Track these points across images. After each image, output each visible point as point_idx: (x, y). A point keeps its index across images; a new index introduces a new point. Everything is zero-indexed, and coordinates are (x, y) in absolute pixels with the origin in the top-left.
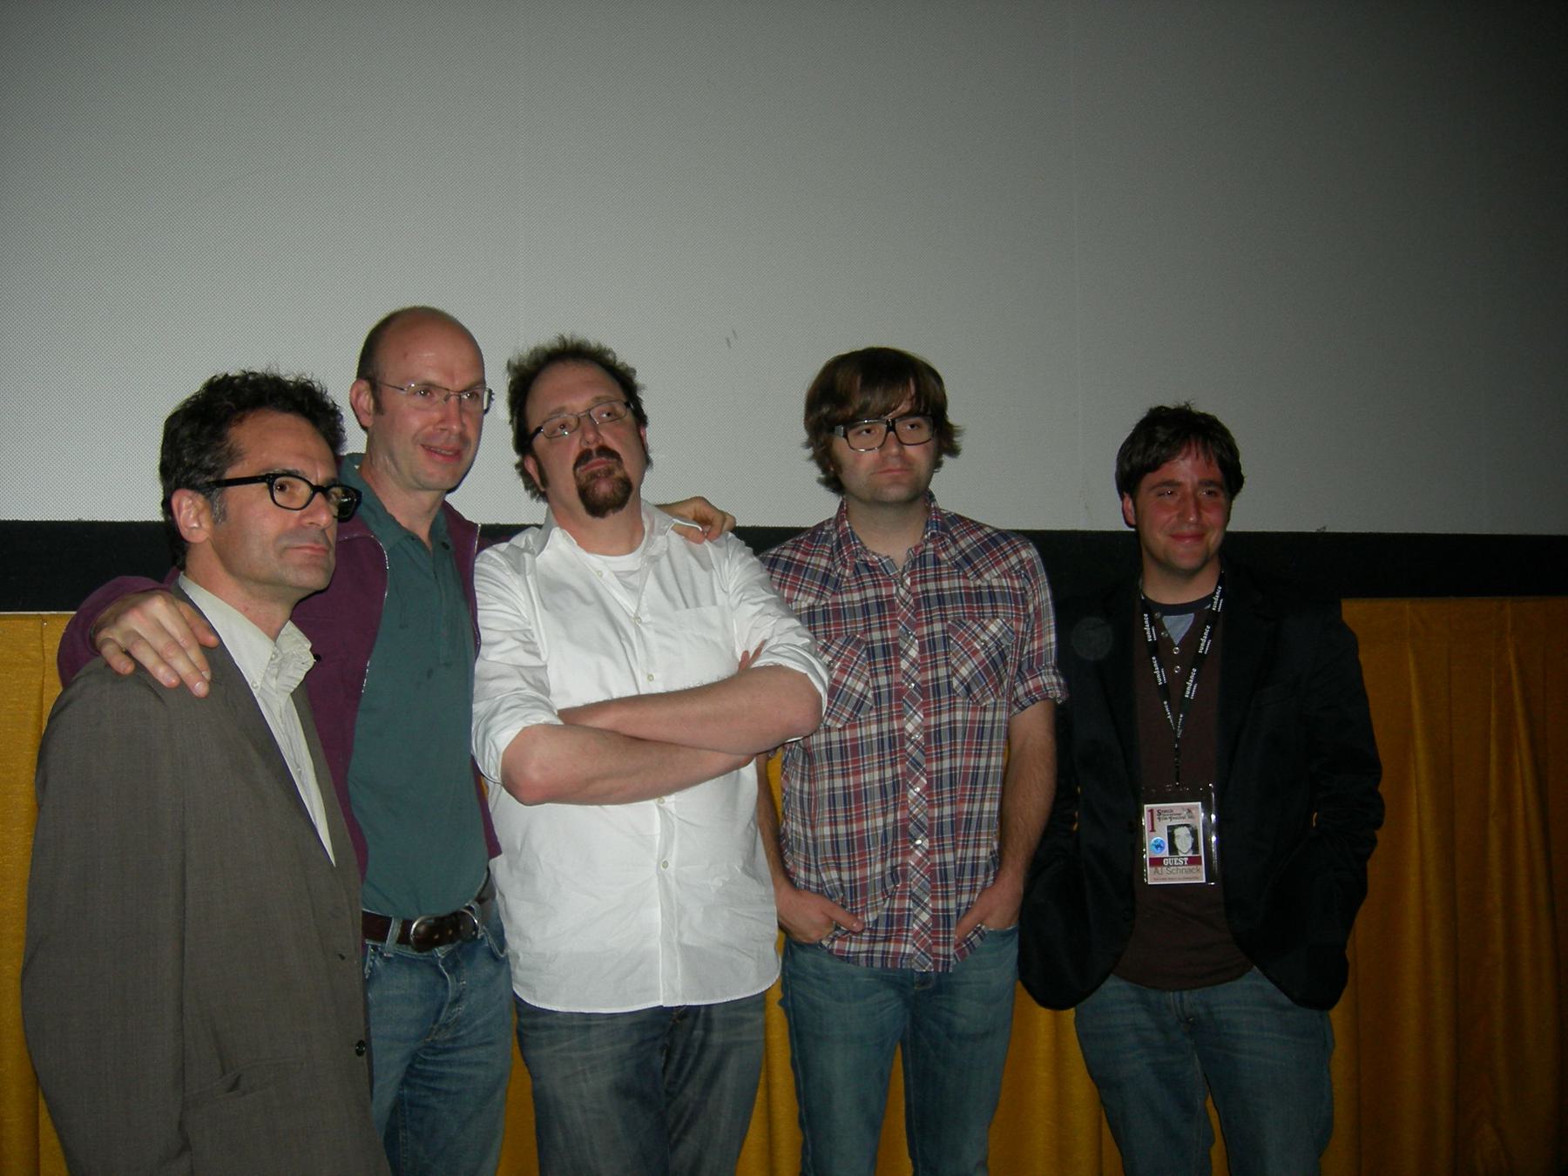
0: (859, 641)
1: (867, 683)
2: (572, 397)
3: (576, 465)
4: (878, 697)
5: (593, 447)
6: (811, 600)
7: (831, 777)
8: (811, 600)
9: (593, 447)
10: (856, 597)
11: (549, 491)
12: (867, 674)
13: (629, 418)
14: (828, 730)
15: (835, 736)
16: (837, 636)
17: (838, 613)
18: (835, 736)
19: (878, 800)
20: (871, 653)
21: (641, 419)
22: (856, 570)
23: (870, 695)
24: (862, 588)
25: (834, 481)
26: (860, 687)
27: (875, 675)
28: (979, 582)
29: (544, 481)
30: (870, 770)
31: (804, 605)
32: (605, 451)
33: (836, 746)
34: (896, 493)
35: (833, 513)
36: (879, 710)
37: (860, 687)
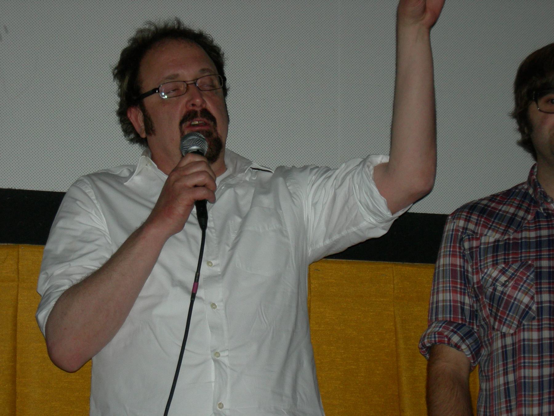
0: (530, 266)
1: (532, 298)
2: (177, 65)
3: (181, 123)
4: (540, 311)
5: (198, 109)
6: (497, 236)
7: (506, 373)
8: (497, 236)
9: (198, 109)
10: (533, 234)
11: (152, 140)
12: (533, 290)
13: (221, 91)
14: (504, 336)
15: (509, 340)
16: (514, 262)
17: (517, 245)
18: (509, 340)
19: (503, 400)
20: (539, 275)
21: (225, 91)
22: (537, 215)
23: (534, 307)
24: (538, 228)
25: (528, 143)
26: (526, 300)
27: (539, 292)
28: (535, 263)
29: (149, 128)
30: (532, 367)
31: (492, 240)
32: (206, 113)
33: (509, 348)
34: (211, 189)
35: (523, 177)
36: (540, 320)
37: (526, 300)
